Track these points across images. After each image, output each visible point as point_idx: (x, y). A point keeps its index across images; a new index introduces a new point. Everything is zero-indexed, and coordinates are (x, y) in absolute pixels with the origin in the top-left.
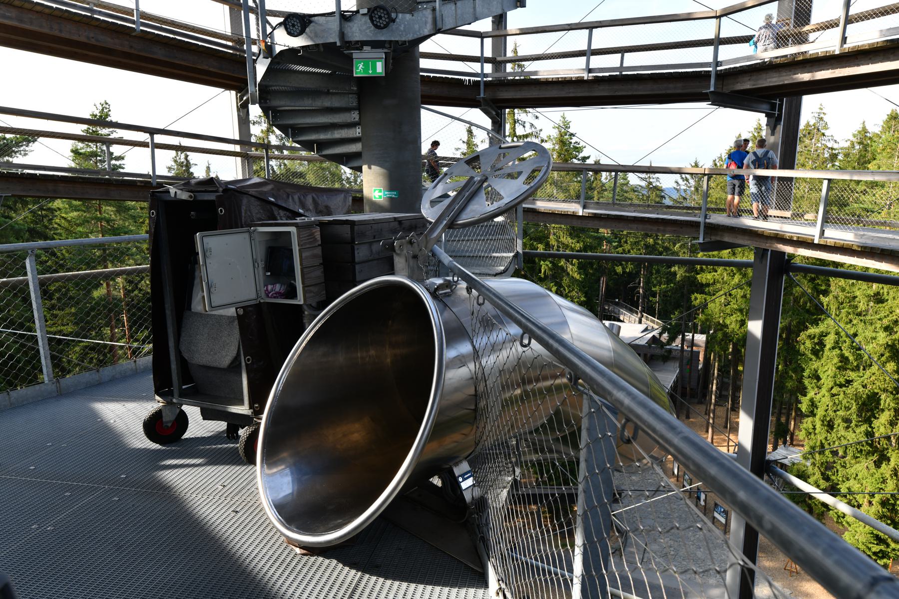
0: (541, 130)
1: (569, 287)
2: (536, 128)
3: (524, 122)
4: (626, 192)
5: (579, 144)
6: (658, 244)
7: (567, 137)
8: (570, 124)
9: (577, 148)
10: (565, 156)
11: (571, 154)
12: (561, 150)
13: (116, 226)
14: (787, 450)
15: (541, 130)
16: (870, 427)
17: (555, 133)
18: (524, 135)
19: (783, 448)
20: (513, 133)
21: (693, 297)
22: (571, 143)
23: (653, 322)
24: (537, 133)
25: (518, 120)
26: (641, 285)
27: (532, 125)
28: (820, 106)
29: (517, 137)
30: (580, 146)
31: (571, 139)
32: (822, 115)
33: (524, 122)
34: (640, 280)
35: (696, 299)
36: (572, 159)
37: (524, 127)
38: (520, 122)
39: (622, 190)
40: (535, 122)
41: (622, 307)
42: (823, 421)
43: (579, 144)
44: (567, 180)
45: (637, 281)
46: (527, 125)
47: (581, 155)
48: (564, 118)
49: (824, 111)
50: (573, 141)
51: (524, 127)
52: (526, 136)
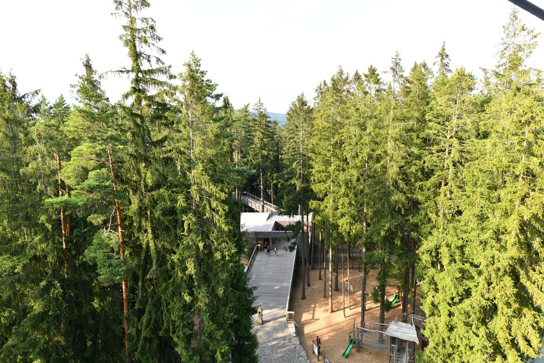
0: (170, 67)
1: (217, 239)
2: (163, 63)
3: (149, 56)
4: (249, 121)
5: (211, 82)
6: (270, 155)
7: (199, 75)
8: (201, 61)
9: (210, 86)
10: (198, 93)
11: (204, 91)
12: (193, 86)
13: (93, 112)
14: (397, 325)
15: (170, 67)
16: (487, 328)
17: (185, 70)
18: (149, 70)
19: (394, 323)
20: (136, 67)
21: (310, 204)
22: (203, 81)
23: (270, 206)
24: (166, 69)
25: (141, 53)
26: (262, 183)
27: (158, 60)
28: (396, 54)
29: (141, 72)
30: (213, 83)
31: (203, 77)
32: (398, 61)
33: (149, 56)
34: (260, 179)
35: (312, 204)
36: (205, 97)
37: (149, 61)
38: (143, 55)
39: (246, 120)
40: (162, 57)
41: (249, 196)
42: (447, 325)
43: (211, 82)
44: (204, 121)
45: (258, 181)
46: (153, 60)
47: (215, 93)
48: (194, 56)
49: (399, 57)
50: (205, 79)
51: (149, 61)
52: (151, 72)
